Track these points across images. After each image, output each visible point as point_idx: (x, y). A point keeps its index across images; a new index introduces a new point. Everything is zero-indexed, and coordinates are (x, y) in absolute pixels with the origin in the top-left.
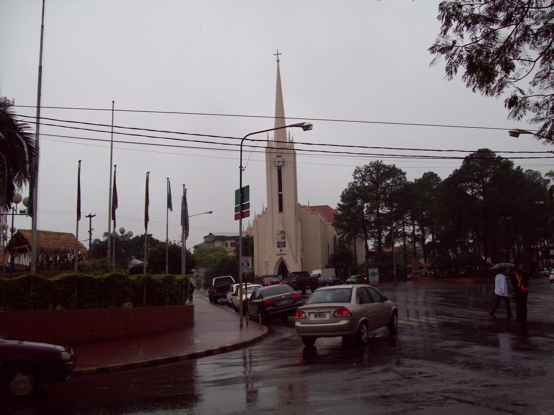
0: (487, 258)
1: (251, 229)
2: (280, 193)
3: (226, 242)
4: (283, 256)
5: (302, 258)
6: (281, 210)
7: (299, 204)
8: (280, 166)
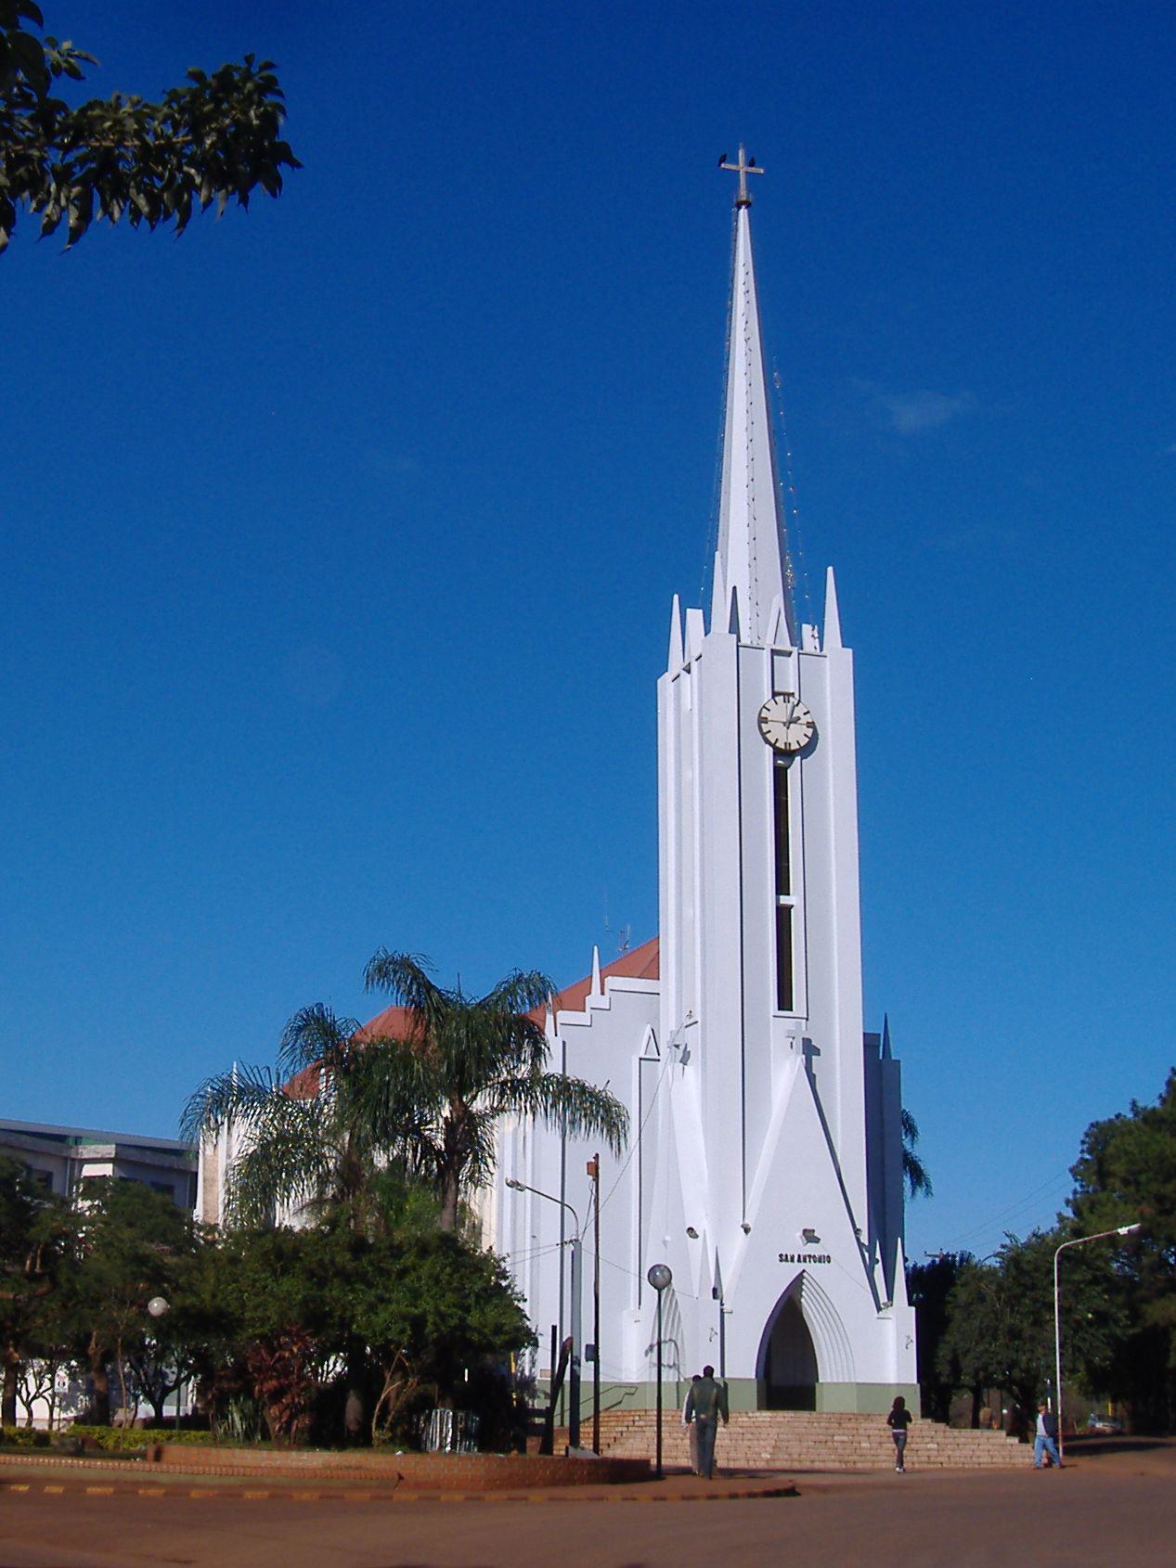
2: (784, 900)
6: (785, 1001)
8: (794, 746)
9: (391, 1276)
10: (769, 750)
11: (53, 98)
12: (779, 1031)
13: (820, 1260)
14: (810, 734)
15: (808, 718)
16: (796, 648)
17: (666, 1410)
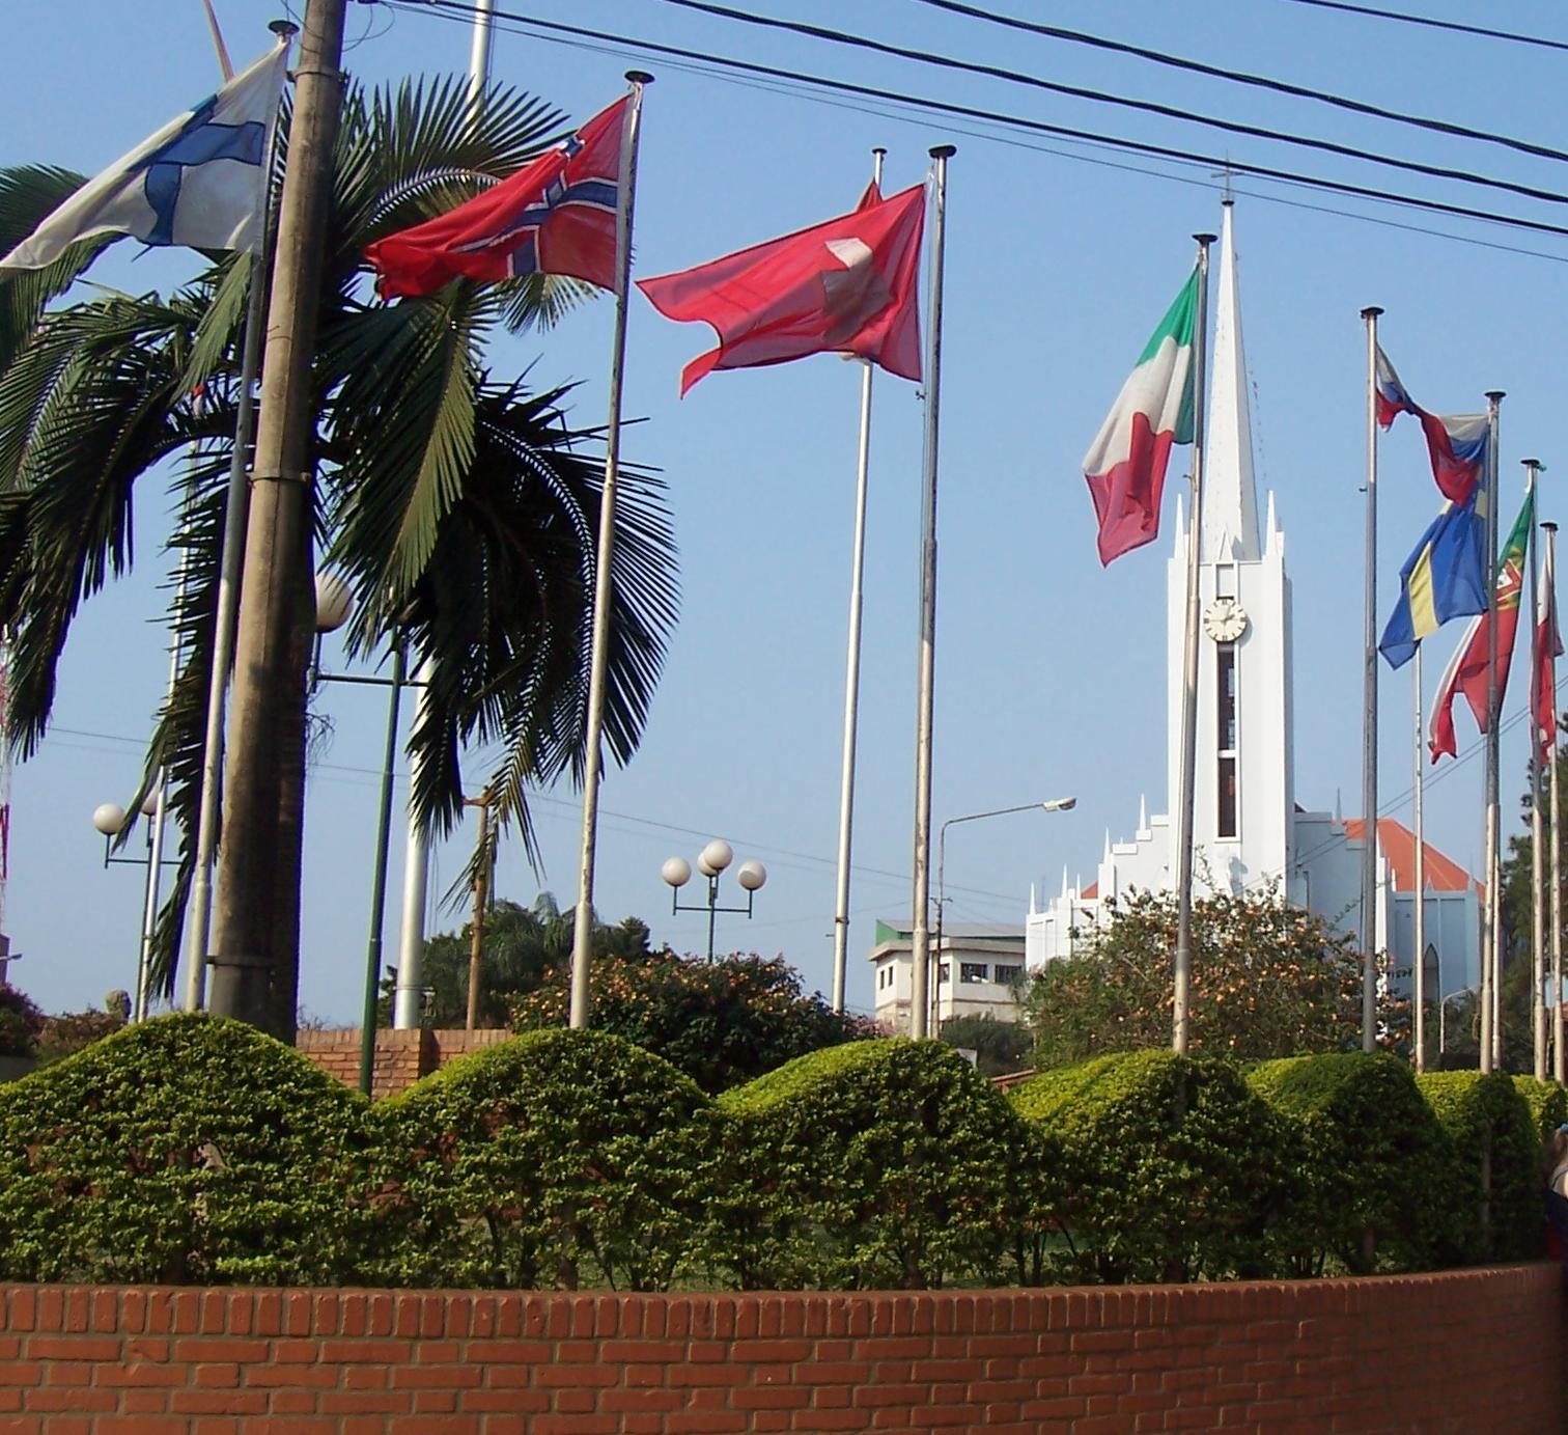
2: (1226, 754)
7: (1298, 809)
8: (1230, 638)
10: (1215, 644)
11: (832, 250)
15: (1242, 615)
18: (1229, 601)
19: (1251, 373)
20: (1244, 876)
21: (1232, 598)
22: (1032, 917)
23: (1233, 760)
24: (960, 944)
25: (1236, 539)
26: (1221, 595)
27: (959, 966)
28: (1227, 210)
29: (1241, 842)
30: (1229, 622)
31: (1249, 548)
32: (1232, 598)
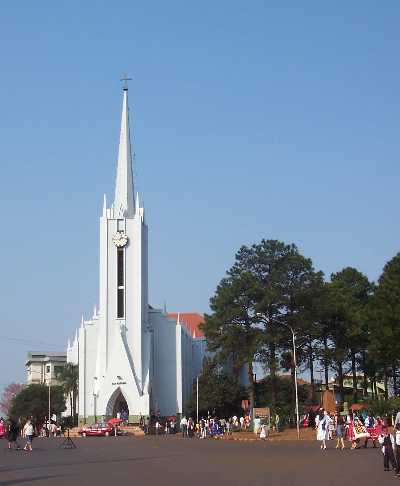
0: (344, 386)
1: (149, 313)
2: (121, 288)
3: (228, 362)
4: (121, 386)
5: (151, 389)
6: (120, 314)
7: (150, 307)
8: (122, 245)
9: (359, 298)
10: (117, 248)
12: (117, 322)
13: (123, 383)
14: (126, 241)
16: (125, 218)
17: (329, 375)
18: (121, 232)
19: (133, 151)
20: (127, 331)
21: (123, 231)
22: (69, 349)
23: (123, 290)
24: (53, 359)
25: (125, 210)
26: (119, 230)
27: (53, 367)
28: (125, 92)
29: (126, 319)
30: (121, 240)
31: (130, 213)
32: (123, 231)
